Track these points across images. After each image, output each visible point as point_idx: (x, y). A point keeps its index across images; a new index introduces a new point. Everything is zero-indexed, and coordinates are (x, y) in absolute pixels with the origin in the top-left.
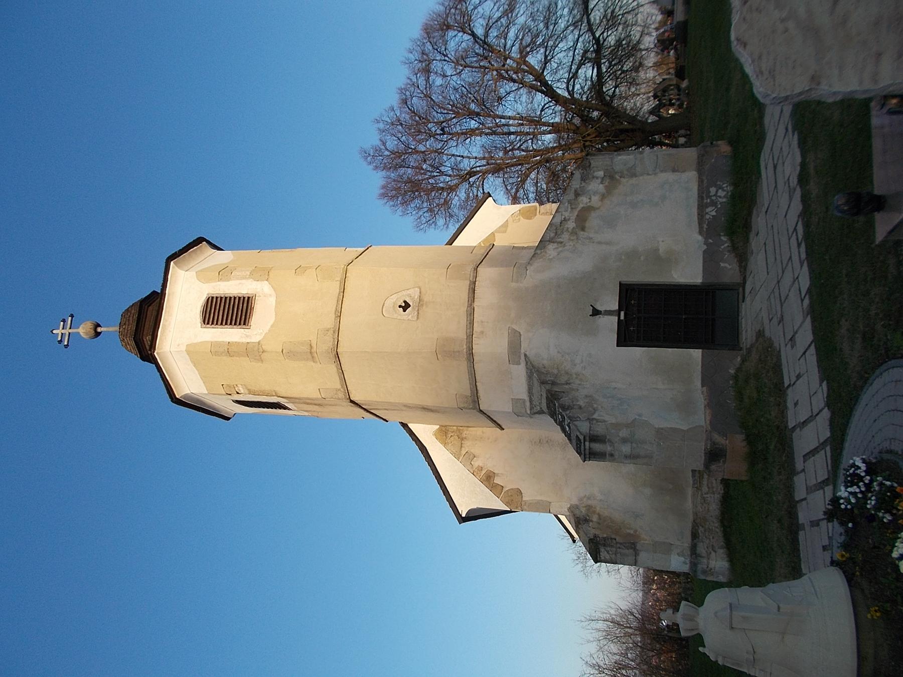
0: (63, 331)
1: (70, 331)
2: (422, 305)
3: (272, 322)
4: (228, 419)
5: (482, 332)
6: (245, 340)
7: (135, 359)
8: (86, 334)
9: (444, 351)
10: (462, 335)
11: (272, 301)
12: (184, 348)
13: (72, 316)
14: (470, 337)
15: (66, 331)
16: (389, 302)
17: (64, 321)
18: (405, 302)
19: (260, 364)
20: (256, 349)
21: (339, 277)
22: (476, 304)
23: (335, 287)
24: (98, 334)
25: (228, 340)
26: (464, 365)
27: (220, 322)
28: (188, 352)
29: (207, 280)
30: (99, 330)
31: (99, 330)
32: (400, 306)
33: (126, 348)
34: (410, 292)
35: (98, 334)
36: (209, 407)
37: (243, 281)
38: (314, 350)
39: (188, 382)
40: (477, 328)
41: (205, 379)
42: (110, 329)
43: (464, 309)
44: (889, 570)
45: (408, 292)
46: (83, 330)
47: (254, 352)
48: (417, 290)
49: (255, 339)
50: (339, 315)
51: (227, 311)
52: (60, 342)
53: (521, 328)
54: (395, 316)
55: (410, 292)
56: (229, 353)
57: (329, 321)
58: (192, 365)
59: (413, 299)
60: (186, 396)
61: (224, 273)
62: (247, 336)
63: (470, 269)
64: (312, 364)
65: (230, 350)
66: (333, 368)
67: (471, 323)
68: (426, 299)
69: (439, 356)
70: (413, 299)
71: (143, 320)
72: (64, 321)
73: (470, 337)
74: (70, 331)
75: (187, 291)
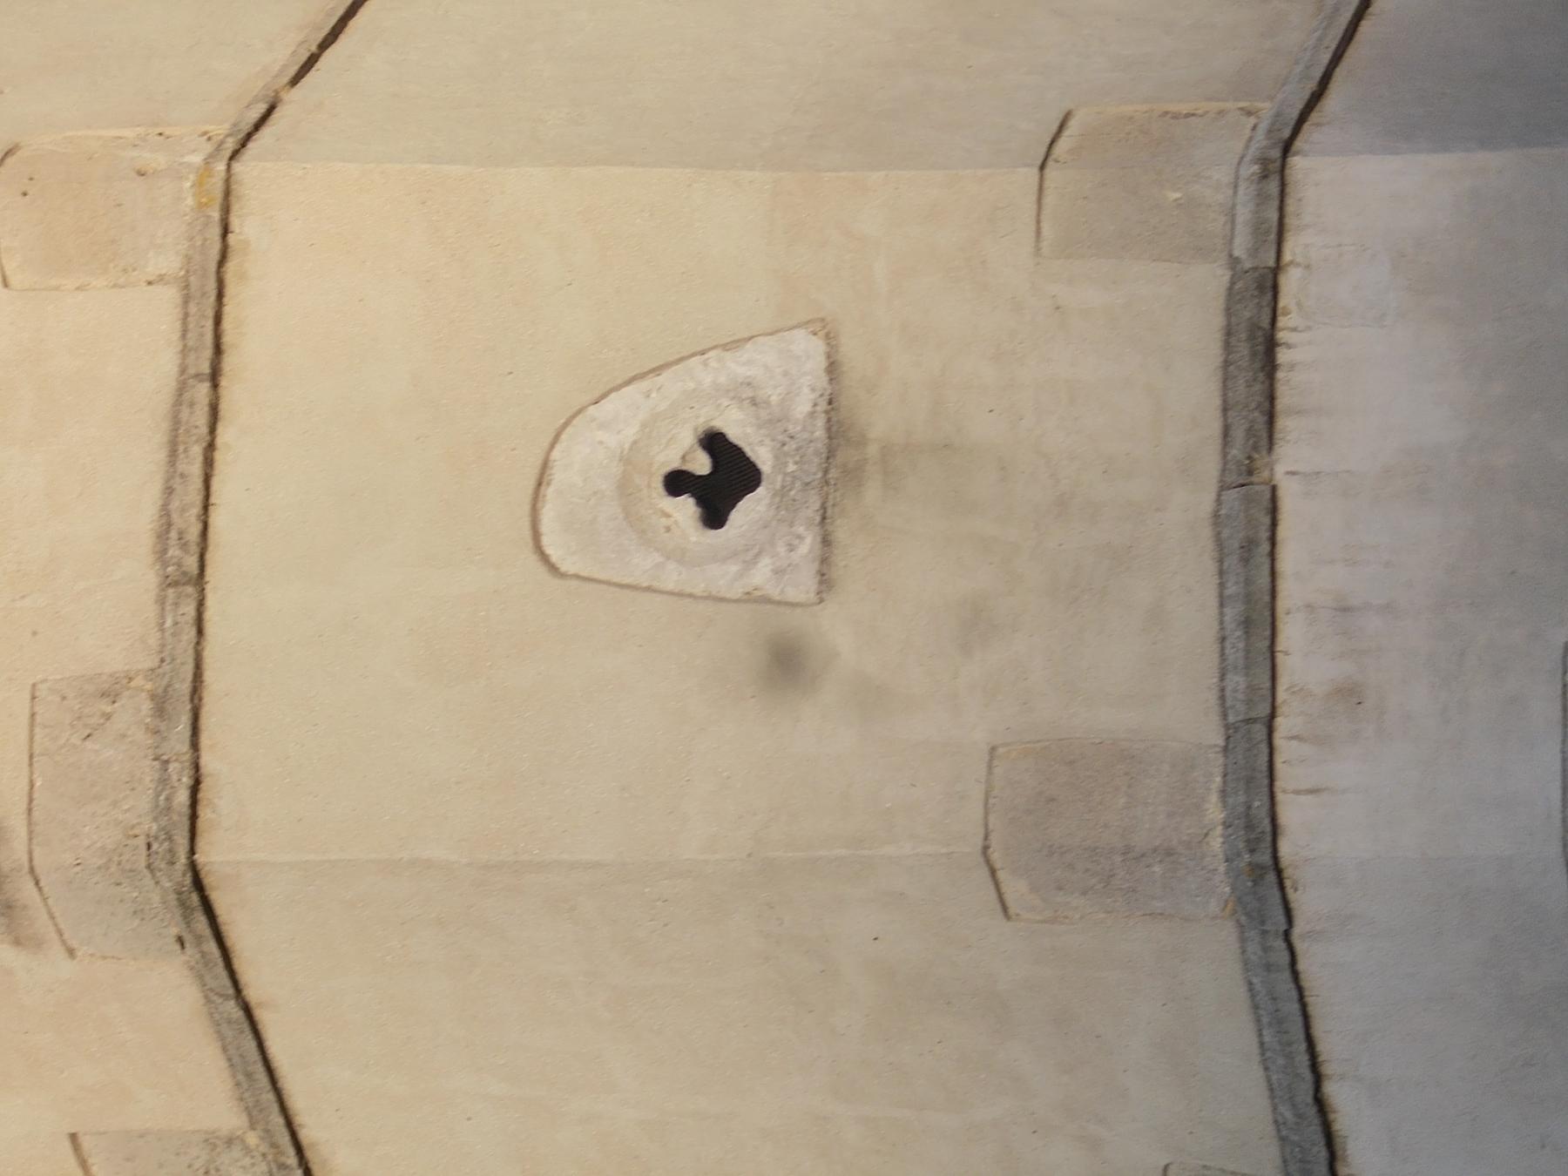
2: (854, 475)
5: (1349, 694)
9: (1051, 833)
10: (1188, 717)
14: (1252, 735)
16: (589, 455)
18: (714, 442)
21: (167, 250)
22: (1291, 460)
23: (140, 337)
26: (1212, 958)
32: (677, 483)
34: (756, 363)
40: (1305, 660)
43: (1192, 502)
44: (170, 569)
45: (739, 366)
48: (808, 350)
50: (188, 571)
53: (214, 816)
54: (641, 565)
55: (756, 363)
57: (115, 620)
59: (775, 422)
63: (1218, 173)
66: (172, 989)
67: (1254, 621)
68: (881, 420)
69: (1015, 888)
70: (775, 422)
73: (1252, 735)
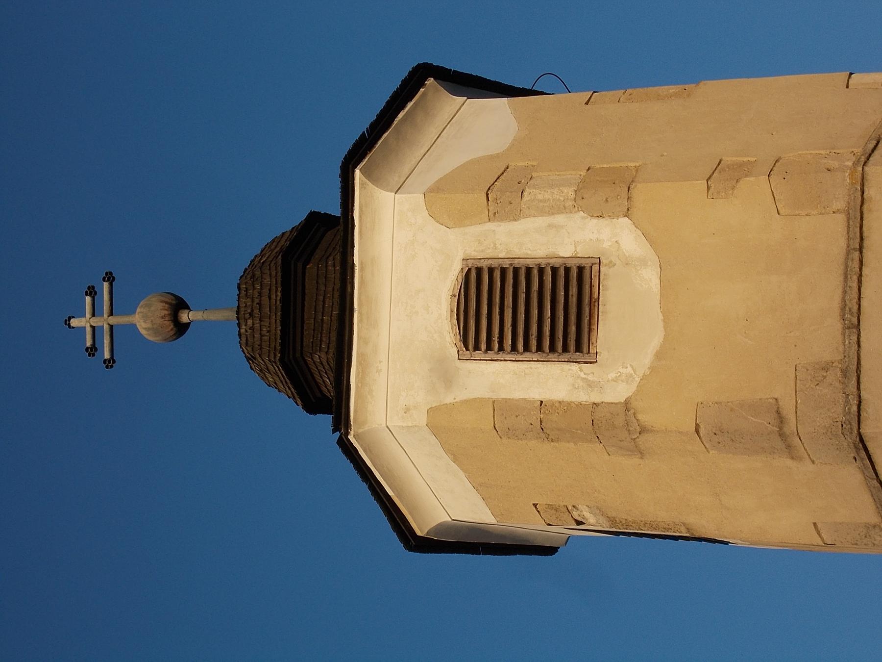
0: (95, 322)
1: (113, 320)
3: (656, 342)
4: (549, 550)
6: (583, 397)
7: (285, 406)
8: (155, 331)
11: (650, 278)
12: (421, 419)
13: (109, 278)
15: (103, 322)
17: (92, 292)
19: (636, 460)
20: (620, 421)
24: (181, 329)
25: (536, 394)
27: (497, 275)
28: (434, 428)
29: (457, 219)
30: (184, 317)
31: (184, 317)
33: (264, 378)
35: (181, 329)
36: (503, 536)
37: (560, 219)
38: (791, 426)
39: (441, 494)
41: (483, 488)
42: (214, 315)
46: (146, 320)
47: (613, 427)
49: (617, 393)
50: (853, 322)
51: (529, 308)
52: (93, 350)
56: (543, 431)
57: (826, 341)
58: (447, 459)
60: (442, 528)
61: (500, 188)
62: (590, 385)
64: (789, 462)
65: (546, 423)
71: (301, 308)
72: (92, 292)
74: (113, 320)
75: (408, 257)
